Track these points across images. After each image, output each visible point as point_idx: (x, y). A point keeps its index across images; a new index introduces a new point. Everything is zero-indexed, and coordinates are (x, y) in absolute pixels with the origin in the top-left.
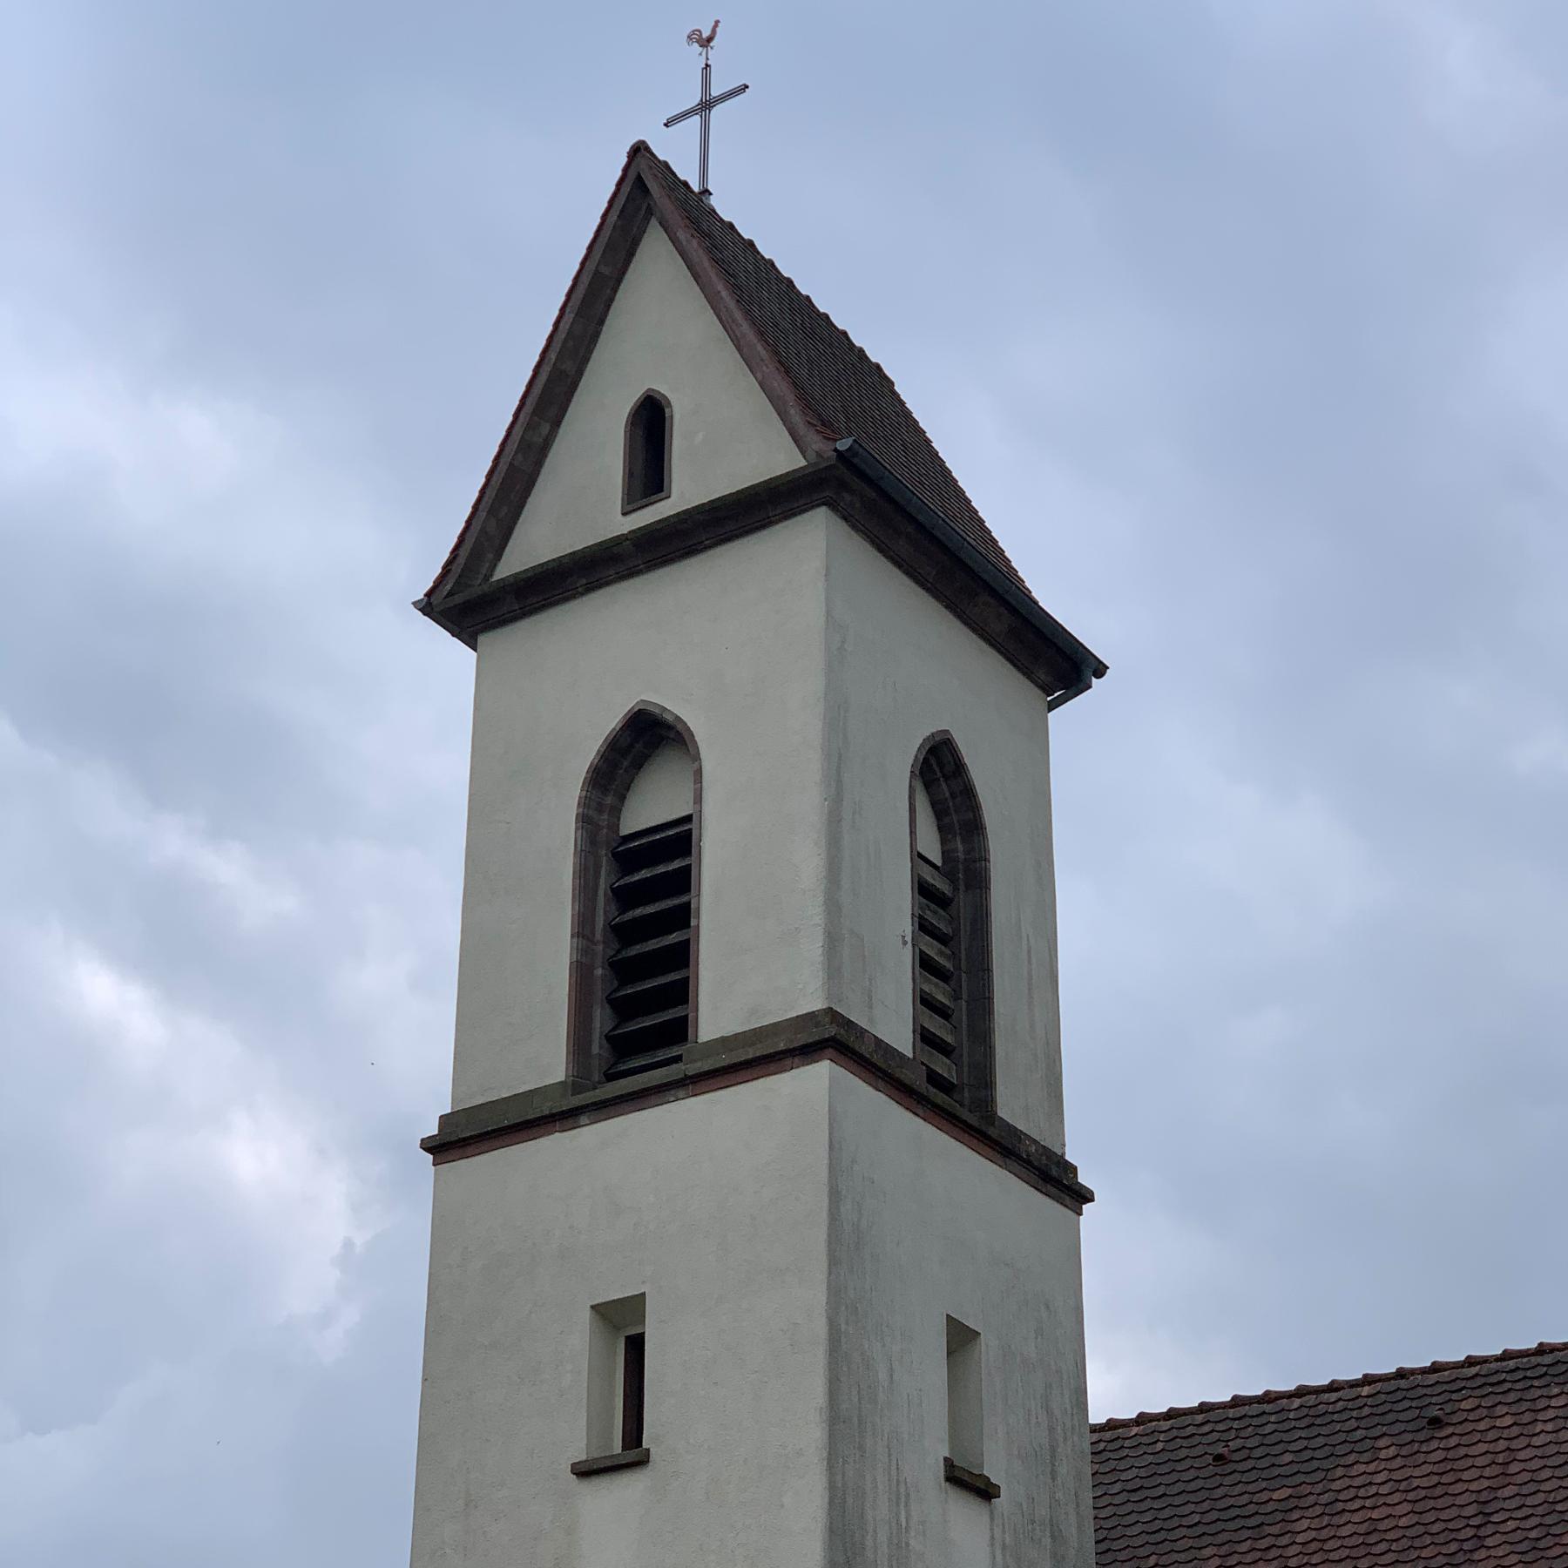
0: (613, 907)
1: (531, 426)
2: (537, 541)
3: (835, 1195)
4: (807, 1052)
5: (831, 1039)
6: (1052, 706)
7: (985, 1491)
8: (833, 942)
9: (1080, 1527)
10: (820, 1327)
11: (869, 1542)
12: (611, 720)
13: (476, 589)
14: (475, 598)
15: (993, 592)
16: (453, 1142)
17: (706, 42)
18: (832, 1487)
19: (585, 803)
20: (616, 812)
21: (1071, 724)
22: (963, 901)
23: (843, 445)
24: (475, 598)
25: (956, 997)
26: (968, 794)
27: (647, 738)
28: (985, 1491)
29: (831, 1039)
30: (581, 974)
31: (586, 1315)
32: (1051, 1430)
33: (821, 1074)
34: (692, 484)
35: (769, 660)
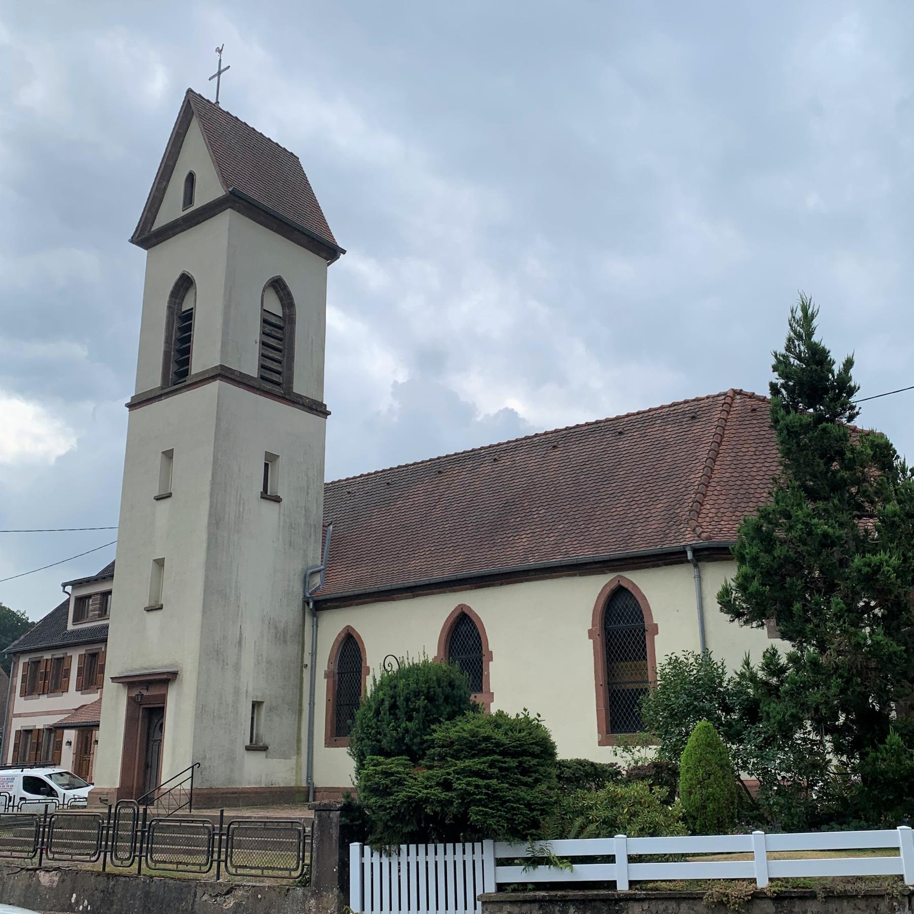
0: (179, 334)
1: (159, 183)
2: (162, 221)
3: (218, 419)
4: (214, 378)
5: (224, 374)
6: (329, 264)
7: (277, 500)
8: (224, 345)
9: (317, 508)
10: (211, 458)
11: (227, 516)
12: (177, 277)
13: (146, 234)
14: (148, 236)
15: (298, 230)
16: (131, 406)
17: (220, 51)
18: (211, 502)
19: (170, 302)
20: (181, 304)
21: (335, 269)
22: (287, 327)
23: (231, 189)
24: (148, 236)
25: (283, 356)
26: (289, 294)
27: (185, 283)
28: (277, 500)
29: (224, 374)
30: (167, 354)
31: (160, 454)
32: (308, 481)
33: (217, 383)
34: (200, 201)
35: (226, 258)
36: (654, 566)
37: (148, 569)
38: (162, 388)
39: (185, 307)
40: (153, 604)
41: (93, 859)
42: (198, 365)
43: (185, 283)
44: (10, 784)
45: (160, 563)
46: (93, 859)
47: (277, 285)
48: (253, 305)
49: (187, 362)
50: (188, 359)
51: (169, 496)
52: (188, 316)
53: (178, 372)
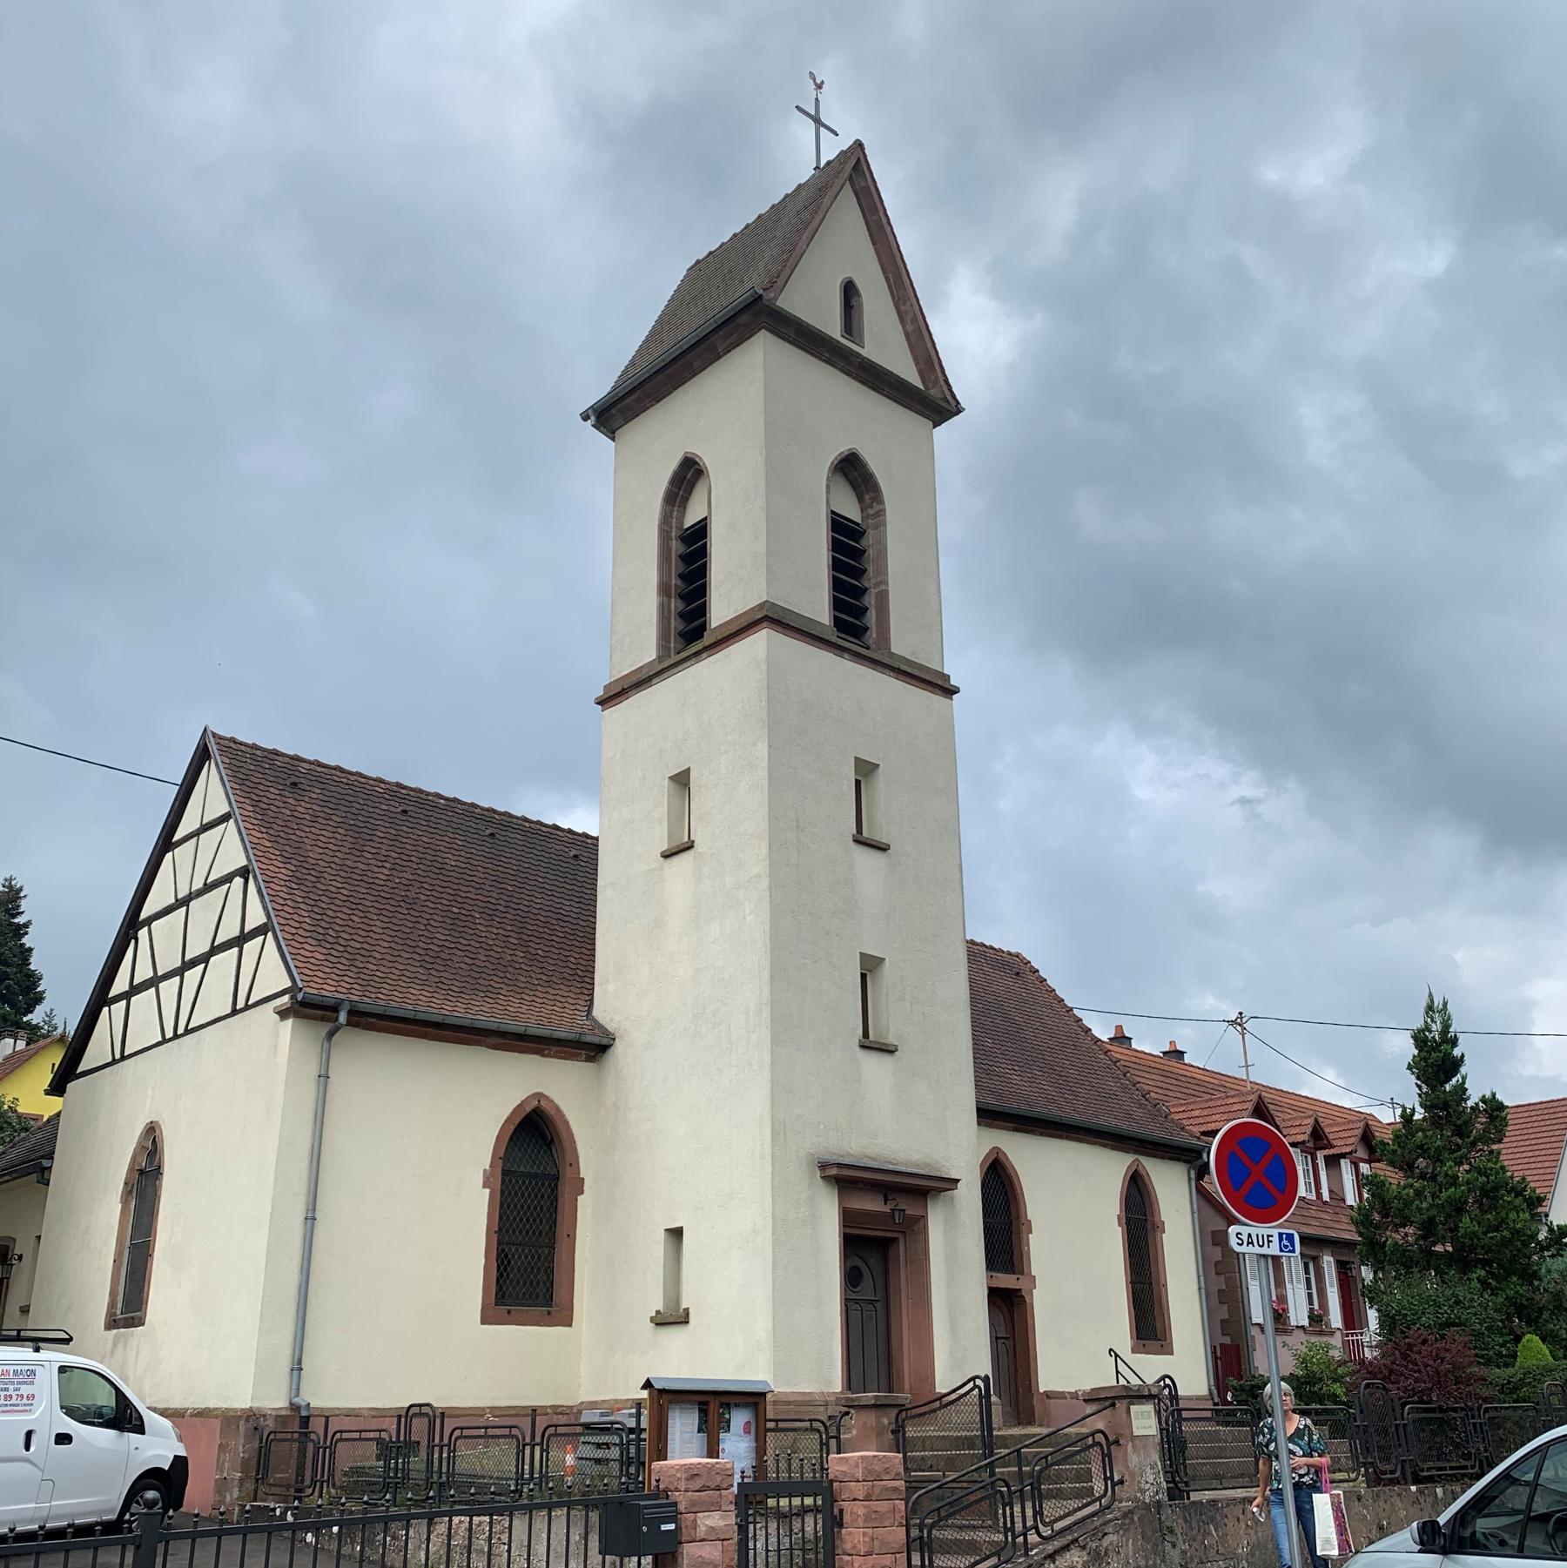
5: (771, 618)
27: (689, 475)
29: (771, 618)
36: (1171, 1159)
37: (658, 1246)
38: (660, 658)
39: (692, 518)
40: (676, 843)
41: (457, 1433)
42: (722, 609)
43: (689, 475)
44: (25, 1390)
45: (676, 1234)
46: (457, 1433)
47: (851, 469)
48: (817, 501)
49: (702, 611)
50: (704, 585)
51: (689, 846)
52: (700, 531)
53: (689, 626)
